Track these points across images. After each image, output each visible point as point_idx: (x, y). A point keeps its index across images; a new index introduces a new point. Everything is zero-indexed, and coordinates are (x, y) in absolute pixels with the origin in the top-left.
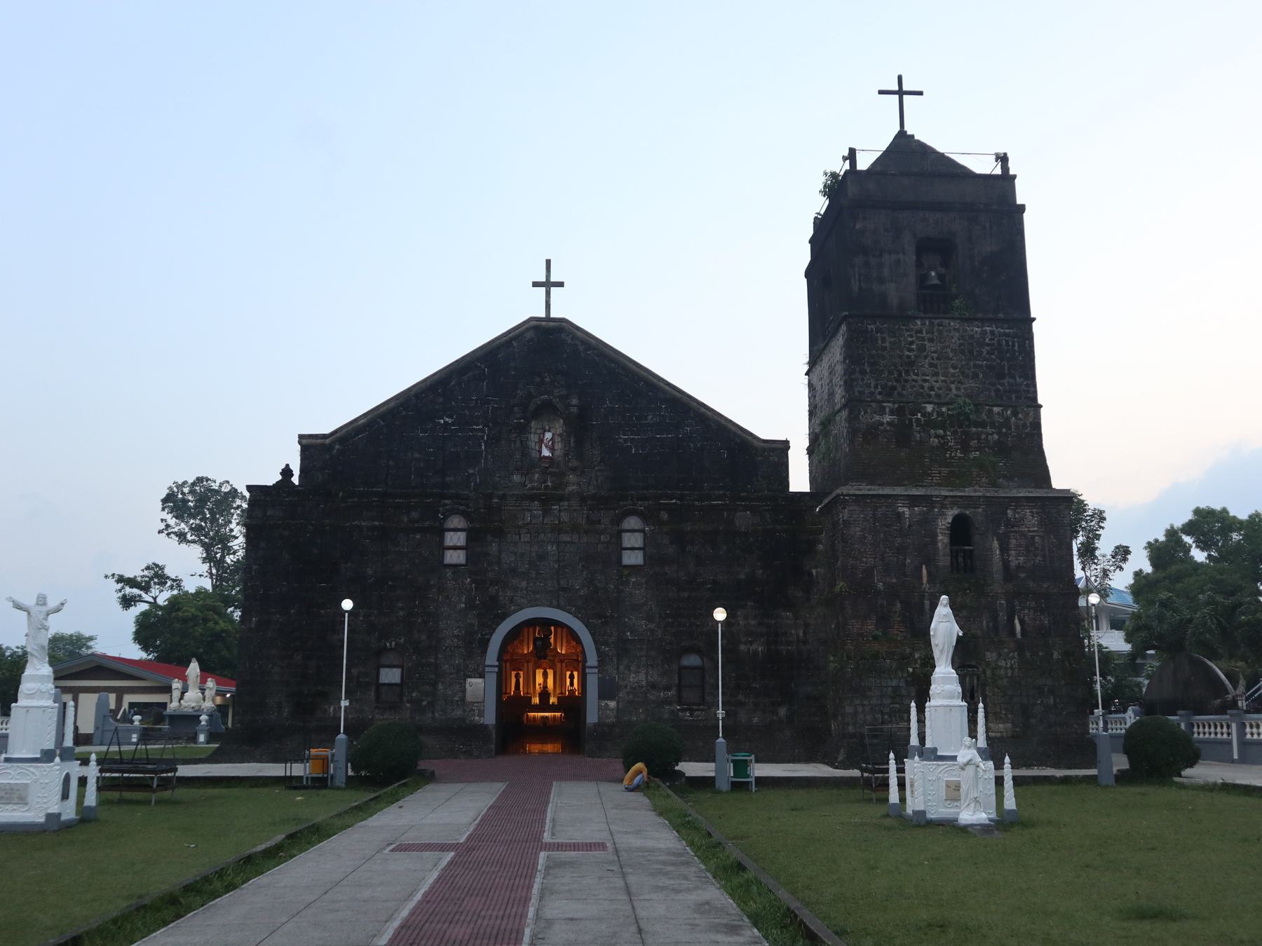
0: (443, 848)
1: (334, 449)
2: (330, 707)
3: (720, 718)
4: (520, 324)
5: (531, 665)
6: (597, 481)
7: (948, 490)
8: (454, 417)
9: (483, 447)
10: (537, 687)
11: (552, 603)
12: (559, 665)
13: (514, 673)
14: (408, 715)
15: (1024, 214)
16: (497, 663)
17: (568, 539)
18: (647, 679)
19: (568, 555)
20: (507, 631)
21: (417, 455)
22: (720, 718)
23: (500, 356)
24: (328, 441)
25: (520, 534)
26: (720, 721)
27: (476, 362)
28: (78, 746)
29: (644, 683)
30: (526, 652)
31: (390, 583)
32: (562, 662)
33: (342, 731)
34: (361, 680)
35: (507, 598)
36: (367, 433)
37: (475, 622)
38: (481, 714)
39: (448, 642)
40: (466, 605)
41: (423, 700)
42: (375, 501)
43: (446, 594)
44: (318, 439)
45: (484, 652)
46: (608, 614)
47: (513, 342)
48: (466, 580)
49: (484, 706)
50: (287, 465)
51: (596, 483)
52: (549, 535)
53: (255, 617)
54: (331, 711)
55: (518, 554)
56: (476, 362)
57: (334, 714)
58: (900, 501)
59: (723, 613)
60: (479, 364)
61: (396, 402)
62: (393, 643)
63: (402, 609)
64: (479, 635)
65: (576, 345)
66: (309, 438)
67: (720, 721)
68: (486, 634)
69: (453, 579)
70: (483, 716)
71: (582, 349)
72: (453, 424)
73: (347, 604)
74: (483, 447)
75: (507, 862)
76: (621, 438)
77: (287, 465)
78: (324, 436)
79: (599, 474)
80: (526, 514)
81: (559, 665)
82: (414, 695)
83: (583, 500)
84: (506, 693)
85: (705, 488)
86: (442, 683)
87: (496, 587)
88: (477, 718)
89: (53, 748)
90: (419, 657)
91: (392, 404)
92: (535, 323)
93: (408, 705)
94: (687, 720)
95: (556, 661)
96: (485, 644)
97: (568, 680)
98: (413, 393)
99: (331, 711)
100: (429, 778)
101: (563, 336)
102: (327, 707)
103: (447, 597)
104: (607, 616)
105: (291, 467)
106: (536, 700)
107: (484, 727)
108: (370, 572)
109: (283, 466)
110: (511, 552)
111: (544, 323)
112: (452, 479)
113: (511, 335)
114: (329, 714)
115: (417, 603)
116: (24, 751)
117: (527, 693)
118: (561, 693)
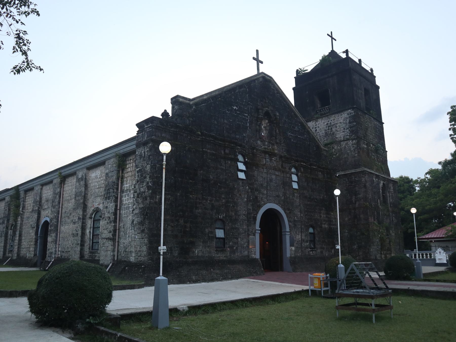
1: (192, 108)
2: (196, 250)
3: (162, 254)
6: (283, 150)
8: (238, 107)
9: (248, 125)
11: (275, 202)
14: (229, 254)
15: (379, 89)
17: (278, 174)
18: (301, 238)
19: (278, 181)
20: (262, 214)
21: (226, 121)
22: (162, 254)
23: (252, 85)
24: (191, 103)
25: (263, 169)
26: (162, 257)
27: (245, 84)
28: (181, 281)
29: (300, 239)
31: (219, 184)
33: (340, 262)
34: (210, 235)
35: (260, 198)
36: (206, 104)
37: (251, 208)
38: (255, 254)
39: (241, 217)
40: (247, 199)
41: (234, 246)
42: (212, 140)
43: (240, 193)
44: (186, 100)
45: (255, 223)
46: (291, 209)
47: (256, 81)
48: (247, 187)
49: (256, 250)
50: (165, 111)
51: (282, 151)
52: (273, 171)
53: (159, 196)
54: (196, 252)
55: (263, 178)
56: (245, 84)
57: (198, 254)
58: (374, 176)
59: (415, 210)
60: (246, 86)
61: (219, 92)
62: (222, 216)
63: (224, 199)
64: (253, 215)
65: (274, 90)
66: (183, 99)
67: (162, 257)
68: (255, 214)
69: (242, 186)
70: (256, 255)
71: (276, 92)
72: (238, 110)
73: (337, 192)
74: (248, 125)
76: (288, 134)
77: (165, 111)
78: (190, 100)
79: (283, 147)
80: (264, 159)
82: (231, 244)
83: (281, 157)
85: (311, 161)
86: (240, 238)
87: (257, 192)
88: (253, 255)
89: (170, 287)
90: (232, 224)
91: (217, 93)
92: (263, 75)
93: (228, 249)
94: (311, 255)
96: (255, 219)
98: (224, 90)
99: (196, 252)
101: (271, 84)
102: (194, 250)
103: (240, 195)
104: (290, 210)
105: (168, 111)
107: (255, 260)
108: (211, 177)
109: (163, 111)
110: (261, 177)
111: (266, 76)
112: (238, 137)
113: (257, 77)
114: (195, 255)
115: (230, 196)
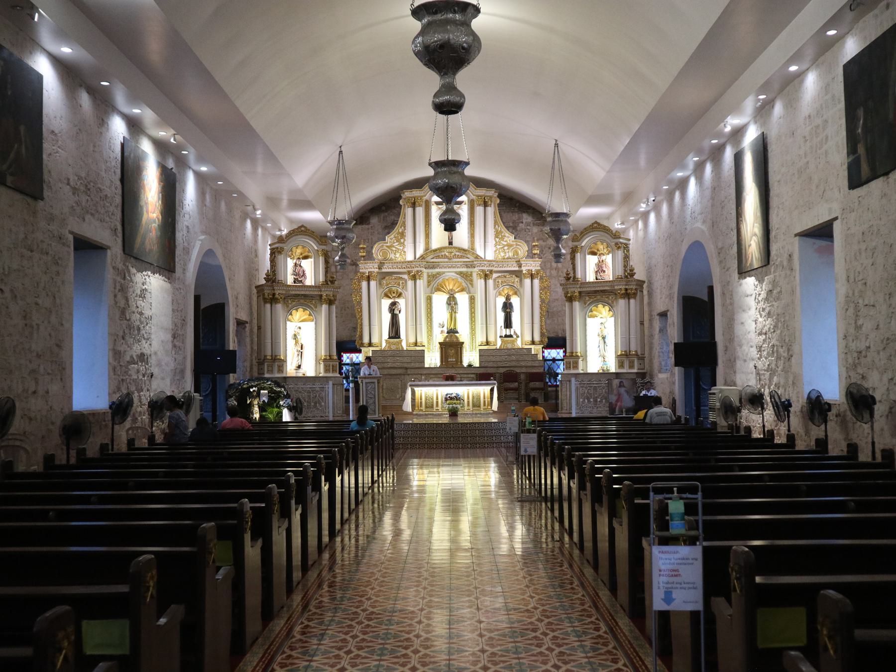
0: (312, 565)
4: (263, 588)
5: (421, 283)
7: (588, 305)
10: (437, 330)
12: (479, 283)
13: (386, 303)
16: (324, 307)
30: (410, 257)
32: (486, 276)
75: (166, 475)
81: (479, 283)
84: (370, 345)
95: (474, 275)
97: (501, 316)
100: (139, 164)
106: (433, 359)
116: (589, 461)
117: (416, 344)
118: (488, 343)
